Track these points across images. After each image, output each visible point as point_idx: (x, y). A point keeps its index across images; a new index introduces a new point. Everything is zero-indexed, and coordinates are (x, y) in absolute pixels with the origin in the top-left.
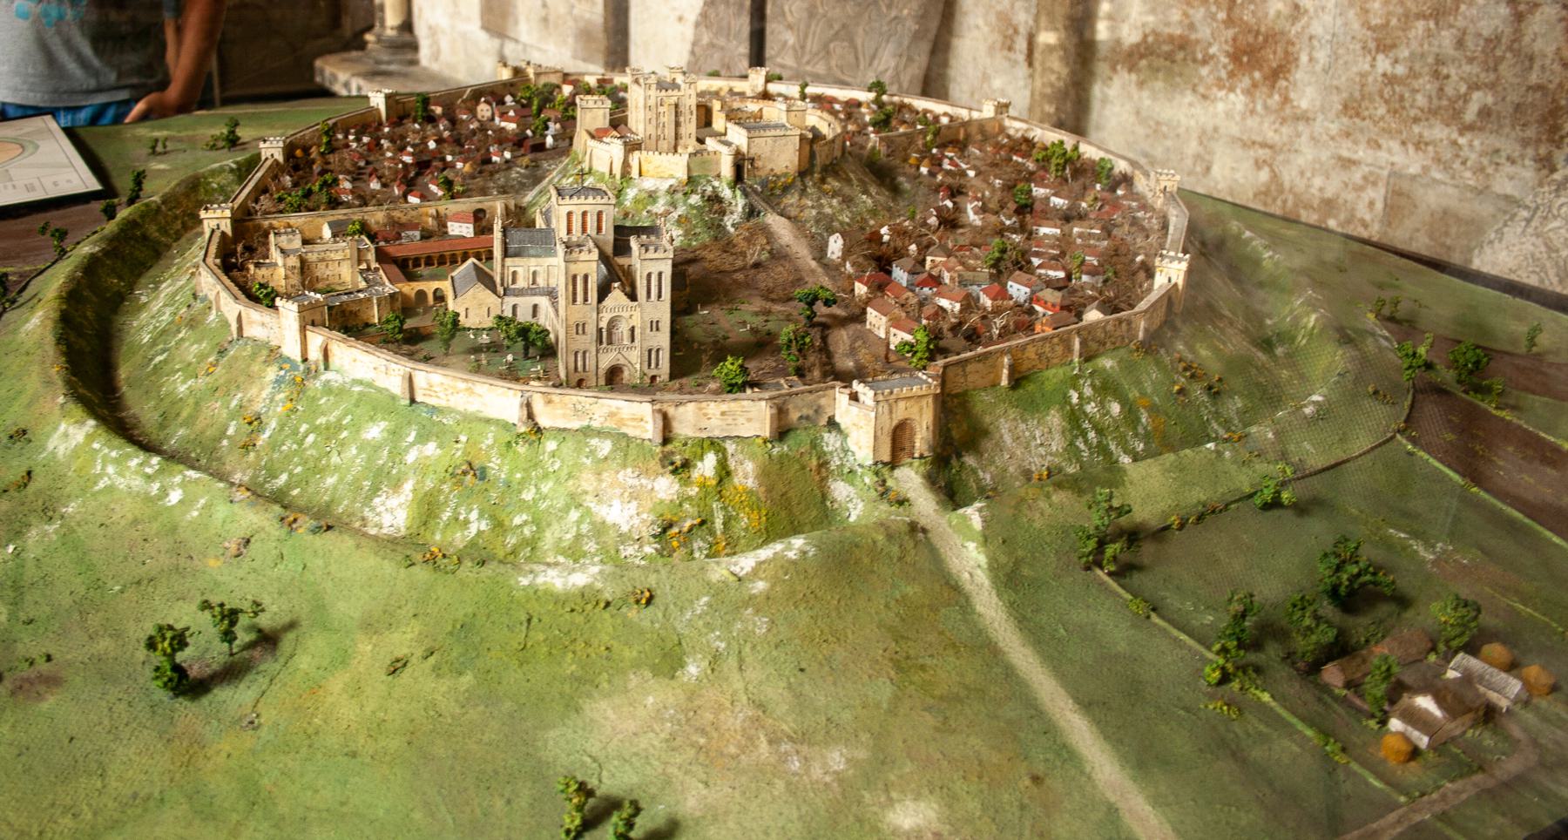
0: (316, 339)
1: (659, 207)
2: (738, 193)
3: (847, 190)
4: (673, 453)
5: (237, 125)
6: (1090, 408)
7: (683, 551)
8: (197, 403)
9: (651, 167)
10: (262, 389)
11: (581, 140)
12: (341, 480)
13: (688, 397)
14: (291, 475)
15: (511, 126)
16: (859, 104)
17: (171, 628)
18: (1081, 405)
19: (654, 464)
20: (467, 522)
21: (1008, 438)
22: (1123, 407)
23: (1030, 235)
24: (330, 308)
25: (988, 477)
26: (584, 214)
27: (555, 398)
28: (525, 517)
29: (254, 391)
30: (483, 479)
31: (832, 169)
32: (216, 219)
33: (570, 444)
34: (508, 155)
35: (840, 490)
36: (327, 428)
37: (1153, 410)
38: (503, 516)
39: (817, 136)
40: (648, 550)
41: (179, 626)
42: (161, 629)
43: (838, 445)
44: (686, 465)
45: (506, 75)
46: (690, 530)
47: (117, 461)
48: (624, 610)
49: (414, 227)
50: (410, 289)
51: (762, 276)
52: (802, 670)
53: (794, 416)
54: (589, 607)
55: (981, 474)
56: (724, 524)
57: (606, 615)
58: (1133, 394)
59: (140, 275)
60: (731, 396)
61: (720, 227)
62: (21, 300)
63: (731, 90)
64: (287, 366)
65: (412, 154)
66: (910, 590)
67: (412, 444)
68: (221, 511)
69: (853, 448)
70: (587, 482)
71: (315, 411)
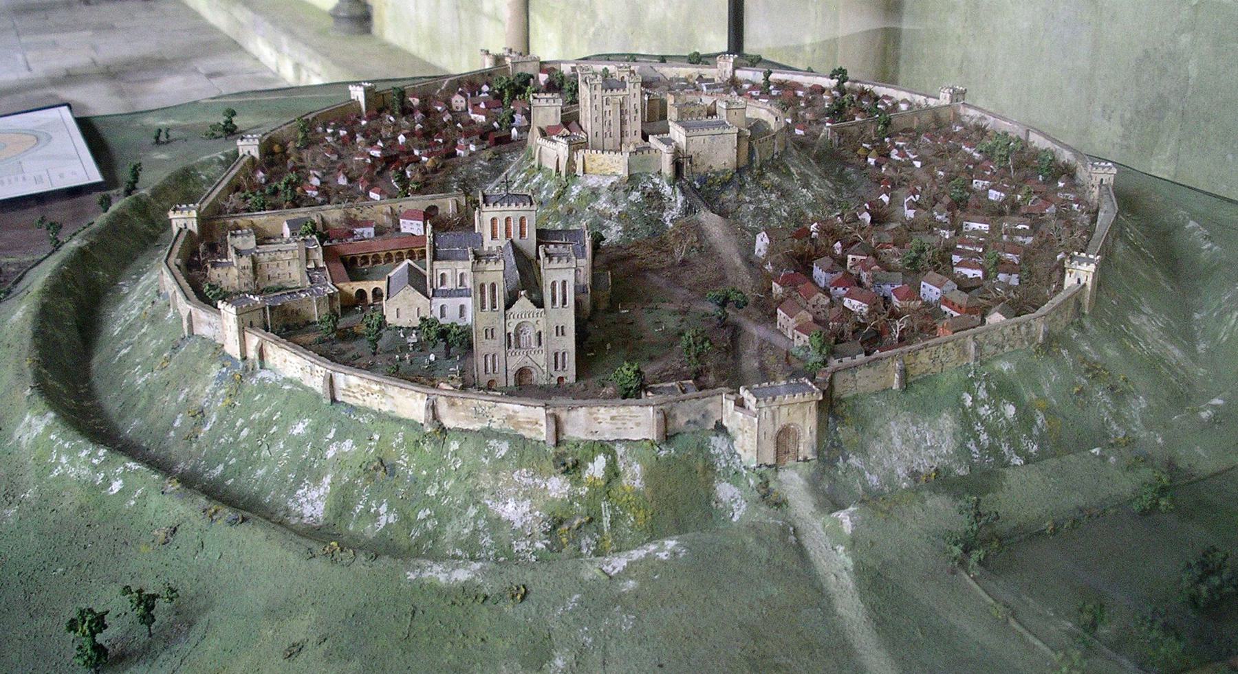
0: (253, 341)
1: (602, 204)
2: (678, 190)
3: (787, 185)
4: (565, 454)
5: (234, 114)
6: (984, 411)
7: (571, 547)
8: (150, 397)
9: (595, 165)
11: (535, 139)
12: (269, 472)
13: (580, 402)
14: (227, 466)
15: (481, 118)
16: (823, 90)
17: (91, 611)
18: (974, 408)
19: (548, 465)
20: (377, 514)
21: (897, 441)
23: (958, 229)
24: (272, 308)
25: (875, 478)
26: (508, 219)
27: (459, 402)
28: (428, 512)
29: (199, 386)
30: (392, 475)
31: (777, 165)
32: (184, 219)
33: (471, 444)
34: (472, 148)
35: (725, 491)
36: (260, 423)
37: (1049, 412)
38: (408, 510)
39: (757, 127)
40: (539, 545)
41: (98, 610)
42: (82, 612)
43: (725, 448)
44: (576, 465)
45: (488, 64)
46: (579, 527)
47: (69, 452)
48: (501, 604)
49: (366, 224)
50: (352, 288)
51: (688, 274)
52: (661, 666)
53: (681, 421)
54: (470, 601)
55: (868, 475)
56: (611, 523)
57: (484, 609)
58: (1029, 396)
59: (124, 267)
60: (624, 401)
61: (659, 223)
62: (15, 291)
63: (700, 76)
64: (229, 364)
65: (382, 149)
66: (775, 591)
67: (332, 441)
68: (155, 501)
69: (740, 451)
70: (486, 480)
71: (249, 408)
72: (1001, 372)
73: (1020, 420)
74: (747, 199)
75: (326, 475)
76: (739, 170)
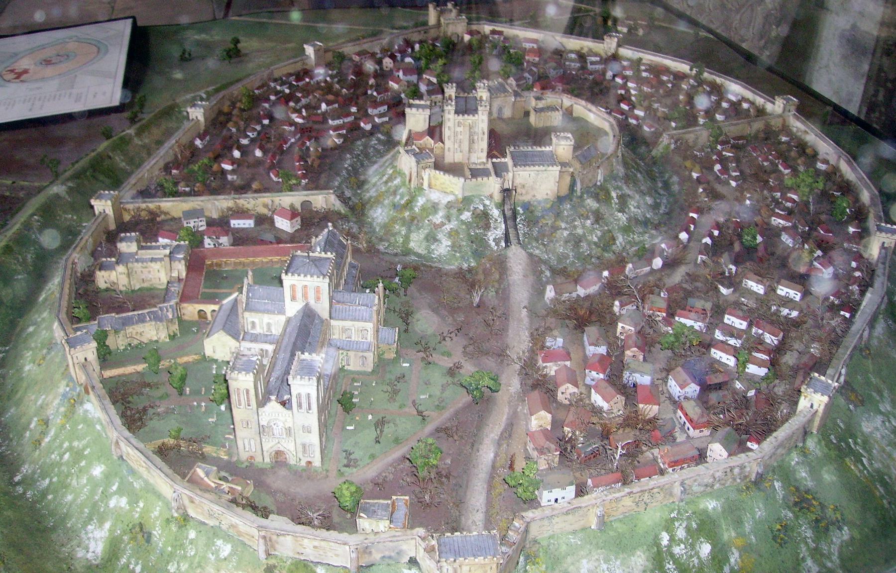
1: (438, 218)
9: (438, 183)
10: (55, 398)
12: (75, 500)
18: (669, 546)
22: (714, 547)
67: (115, 493)
72: (705, 511)
73: (713, 559)
74: (563, 225)
75: (107, 520)
76: (560, 199)
